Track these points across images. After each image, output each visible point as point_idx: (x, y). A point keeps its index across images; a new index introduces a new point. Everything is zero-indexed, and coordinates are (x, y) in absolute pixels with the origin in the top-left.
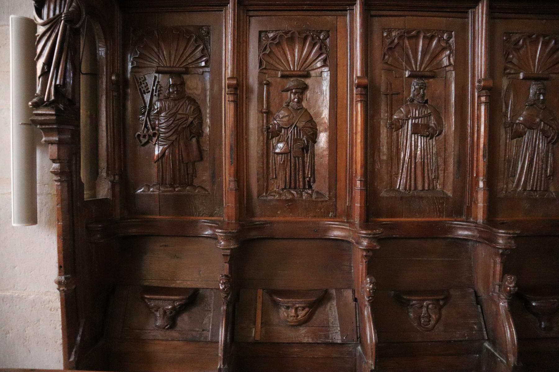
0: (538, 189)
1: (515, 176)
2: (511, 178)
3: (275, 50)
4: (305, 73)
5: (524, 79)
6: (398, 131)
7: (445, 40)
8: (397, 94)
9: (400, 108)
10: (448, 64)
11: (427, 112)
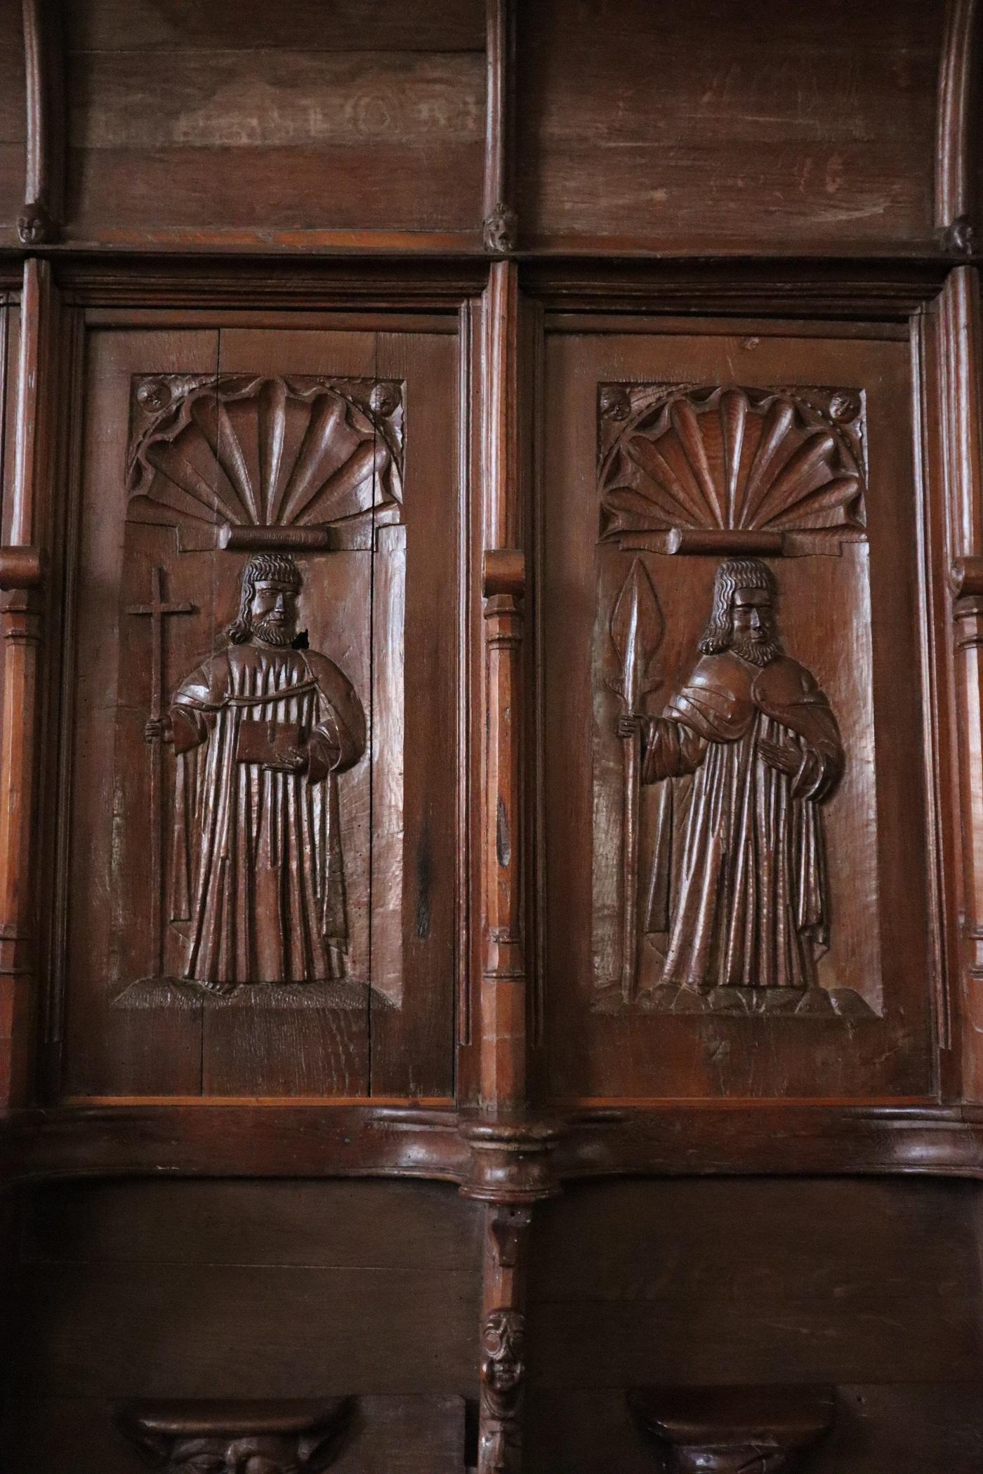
0: (764, 979)
1: (667, 929)
4: (321, 536)
5: (681, 551)
6: (190, 755)
7: (374, 413)
8: (189, 613)
9: (198, 666)
10: (379, 499)
11: (300, 678)
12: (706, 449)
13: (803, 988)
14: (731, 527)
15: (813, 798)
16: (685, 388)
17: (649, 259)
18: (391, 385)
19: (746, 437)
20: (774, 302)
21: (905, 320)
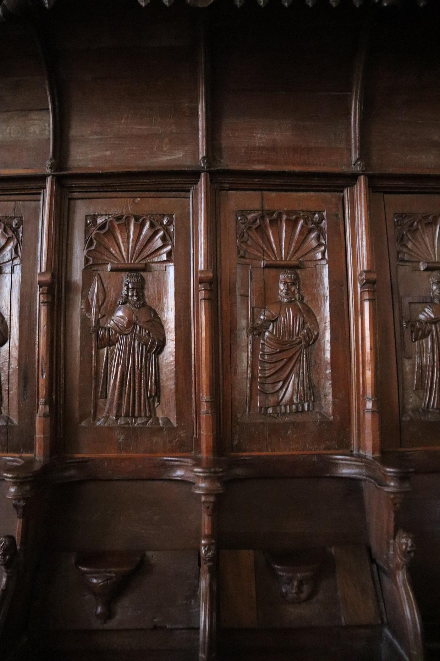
2: (101, 400)
3: (107, 241)
5: (112, 270)
7: (14, 228)
12: (121, 236)
13: (150, 417)
14: (126, 262)
15: (154, 353)
16: (114, 216)
17: (97, 173)
18: (19, 219)
19: (134, 231)
20: (144, 186)
21: (189, 191)
